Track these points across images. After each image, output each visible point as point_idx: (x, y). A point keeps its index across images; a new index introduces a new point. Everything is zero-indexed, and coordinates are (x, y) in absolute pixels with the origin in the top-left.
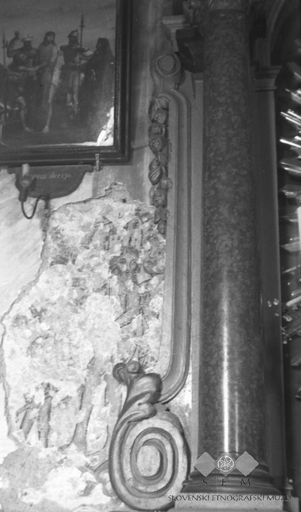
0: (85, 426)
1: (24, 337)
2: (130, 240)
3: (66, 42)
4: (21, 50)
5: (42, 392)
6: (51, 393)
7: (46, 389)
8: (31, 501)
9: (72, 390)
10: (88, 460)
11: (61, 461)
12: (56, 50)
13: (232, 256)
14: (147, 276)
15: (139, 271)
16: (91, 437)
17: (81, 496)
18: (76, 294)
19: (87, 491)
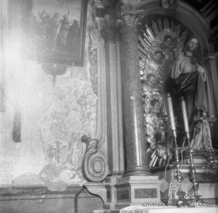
0: (71, 156)
1: (48, 124)
2: (84, 94)
3: (62, 18)
4: (45, 18)
5: (56, 144)
6: (59, 144)
7: (57, 143)
8: (54, 181)
9: (66, 144)
10: (73, 167)
11: (64, 168)
12: (58, 20)
13: (139, 107)
14: (90, 106)
15: (87, 104)
16: (74, 159)
17: (72, 179)
18: (66, 111)
19: (74, 177)
